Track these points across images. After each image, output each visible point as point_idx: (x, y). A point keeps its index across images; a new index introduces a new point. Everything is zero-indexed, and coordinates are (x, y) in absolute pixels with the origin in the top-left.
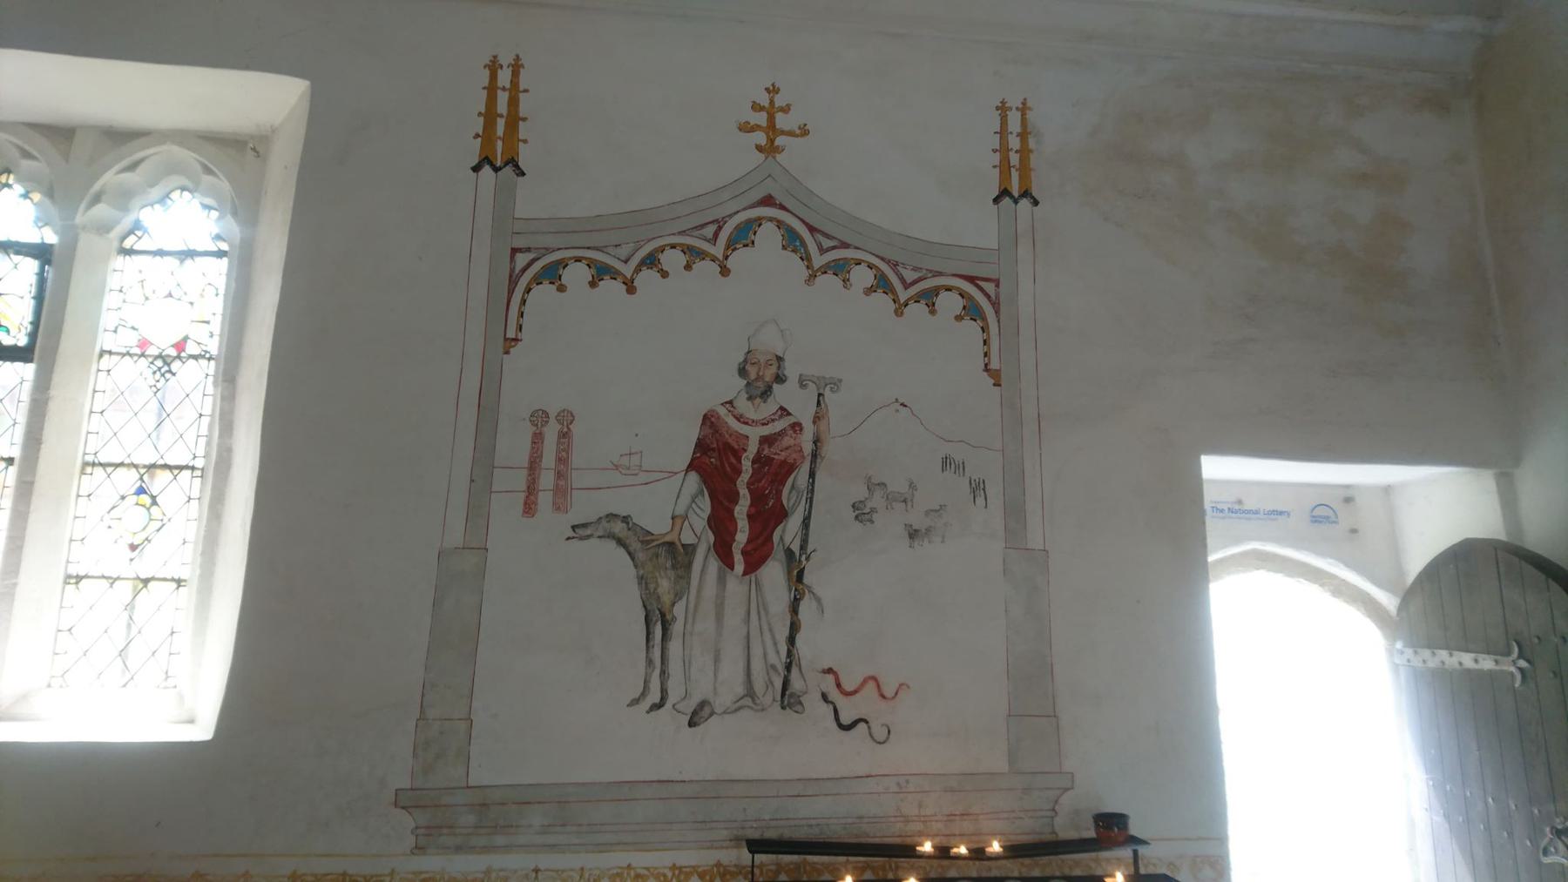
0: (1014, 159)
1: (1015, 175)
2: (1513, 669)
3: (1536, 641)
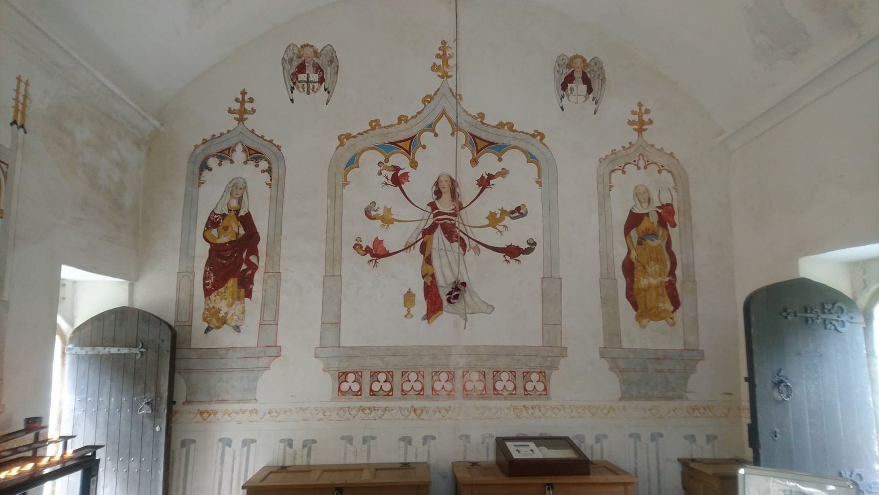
0: (20, 107)
1: (20, 115)
2: (138, 352)
3: (151, 342)
